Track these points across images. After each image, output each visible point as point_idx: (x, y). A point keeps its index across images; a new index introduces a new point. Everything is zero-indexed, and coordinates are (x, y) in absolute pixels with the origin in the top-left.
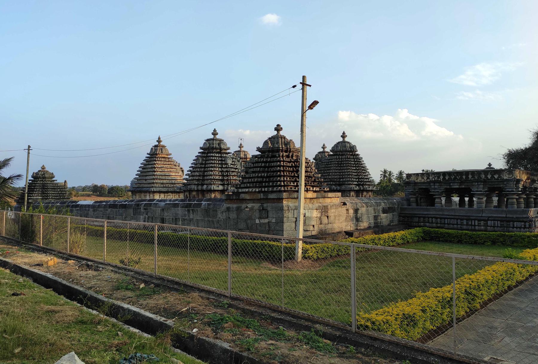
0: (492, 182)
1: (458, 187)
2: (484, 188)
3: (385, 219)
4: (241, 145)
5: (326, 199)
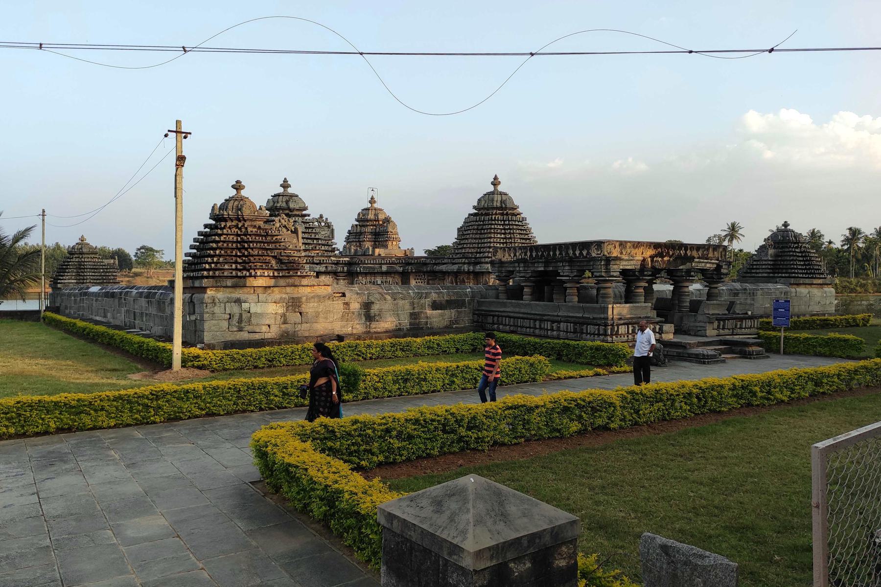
0: (581, 262)
1: (542, 269)
2: (571, 271)
3: (436, 317)
4: (372, 198)
5: (300, 288)
